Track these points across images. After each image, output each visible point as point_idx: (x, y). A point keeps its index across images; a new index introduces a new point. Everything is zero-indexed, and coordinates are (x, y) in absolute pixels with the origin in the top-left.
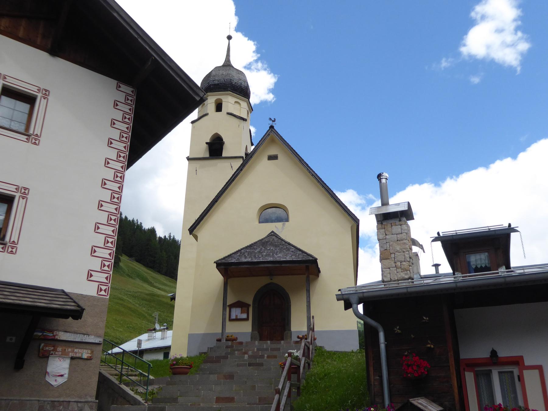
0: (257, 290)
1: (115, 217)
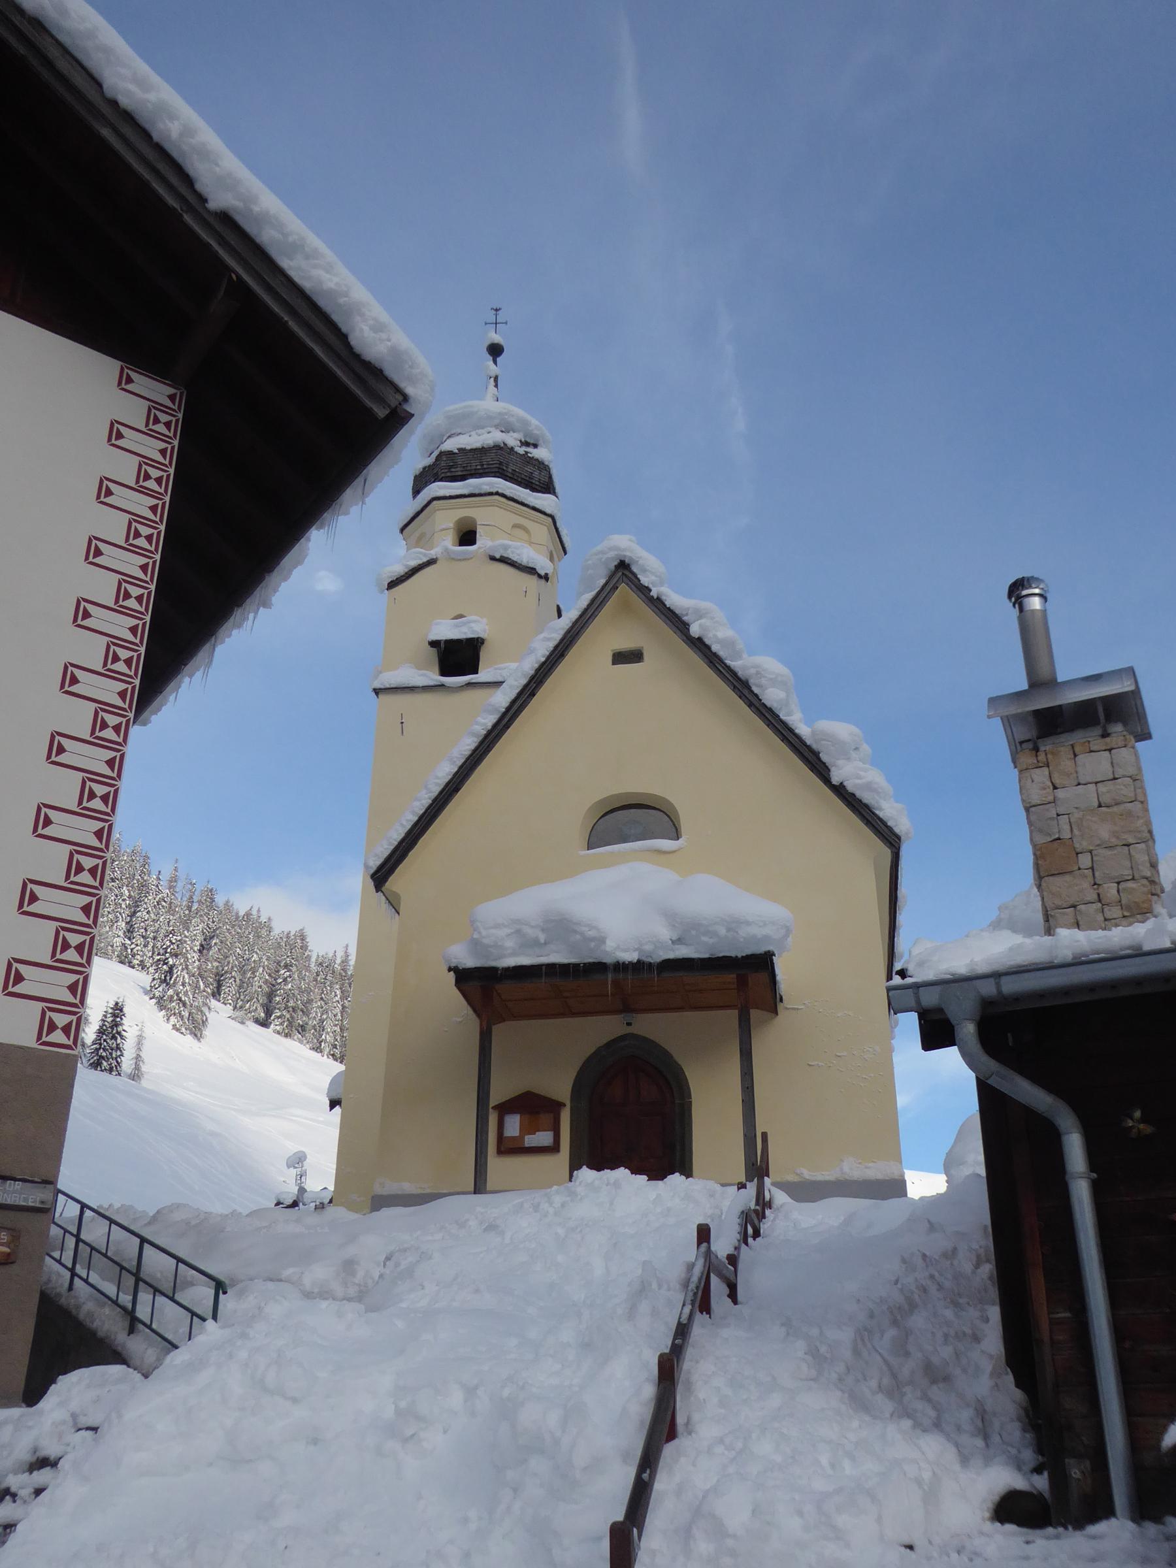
0: (584, 1059)
1: (141, 591)
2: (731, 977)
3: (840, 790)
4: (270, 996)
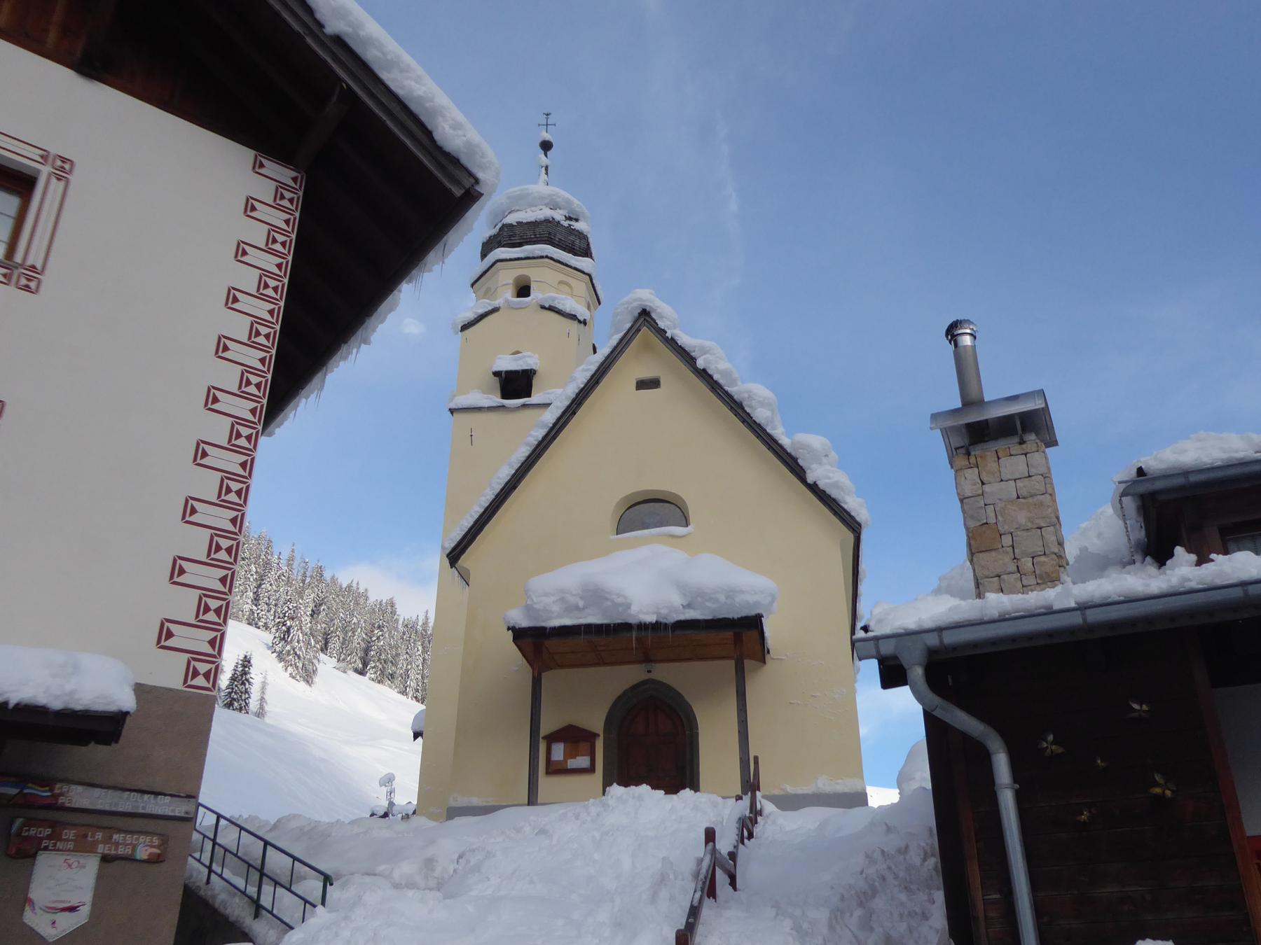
0: (614, 698)
2: (729, 634)
3: (814, 488)
4: (367, 651)
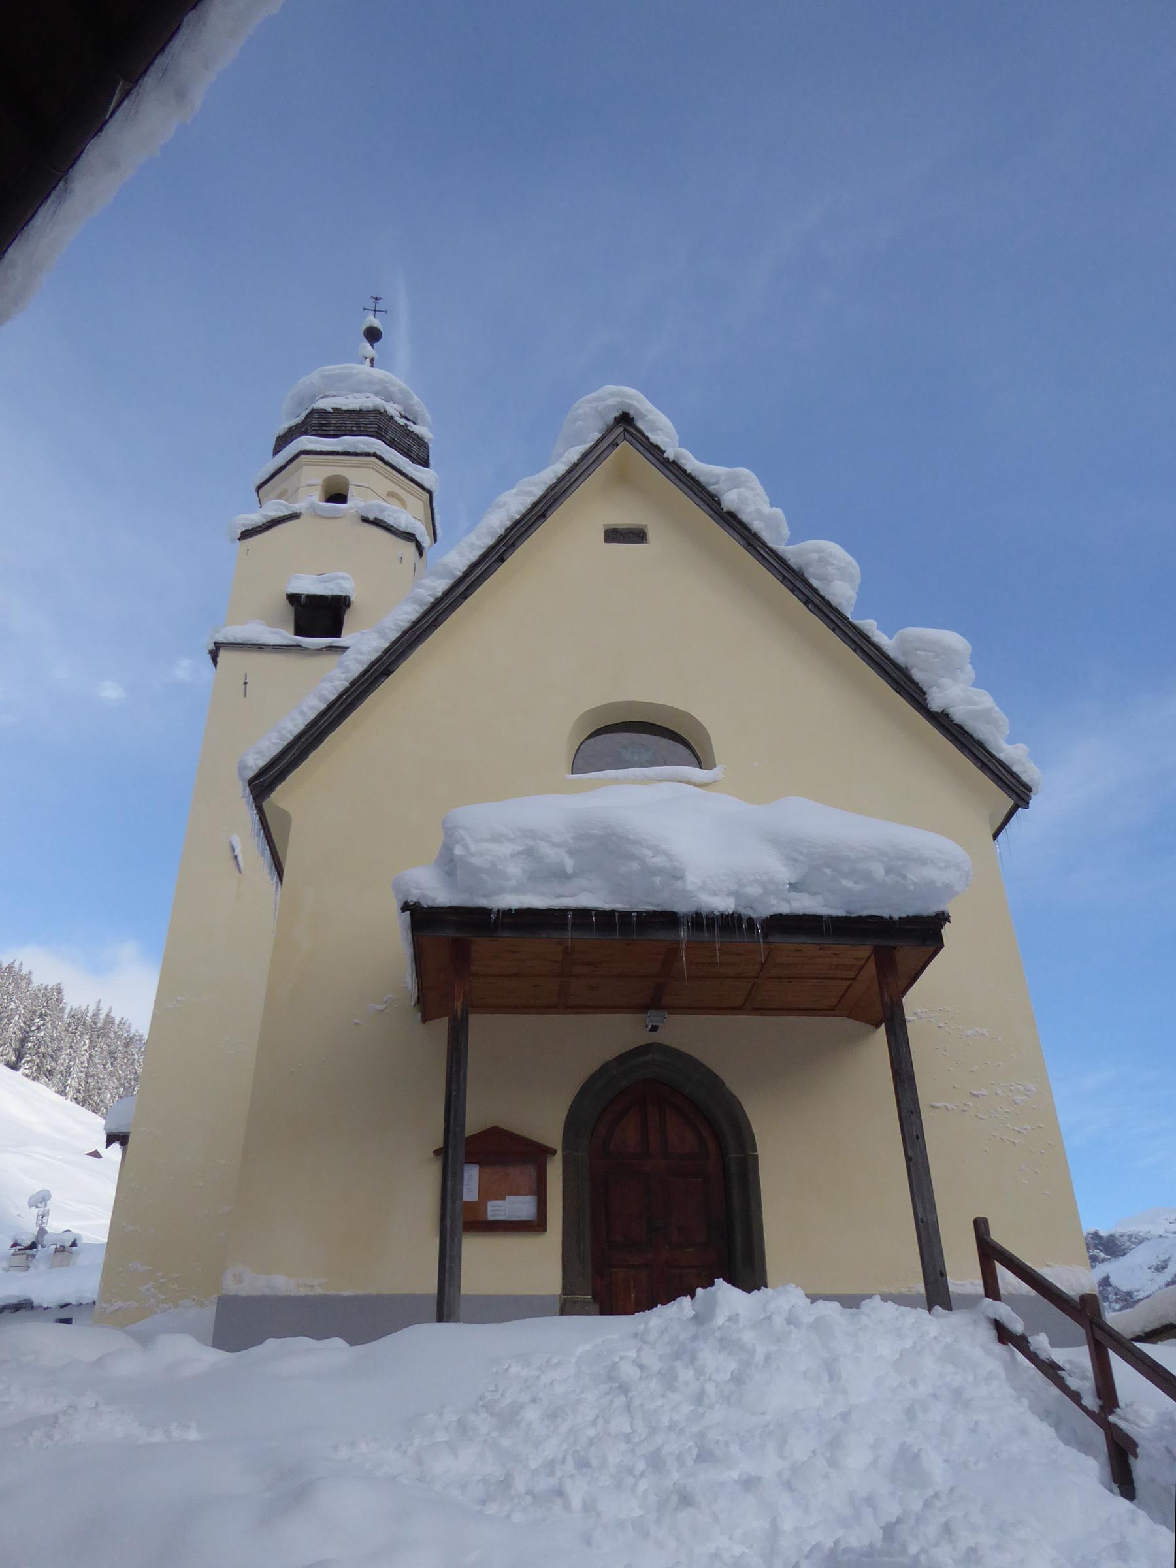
2: (863, 951)
3: (943, 722)
4: (23, 1042)
